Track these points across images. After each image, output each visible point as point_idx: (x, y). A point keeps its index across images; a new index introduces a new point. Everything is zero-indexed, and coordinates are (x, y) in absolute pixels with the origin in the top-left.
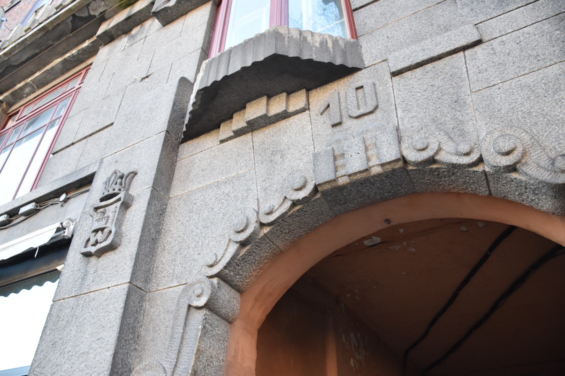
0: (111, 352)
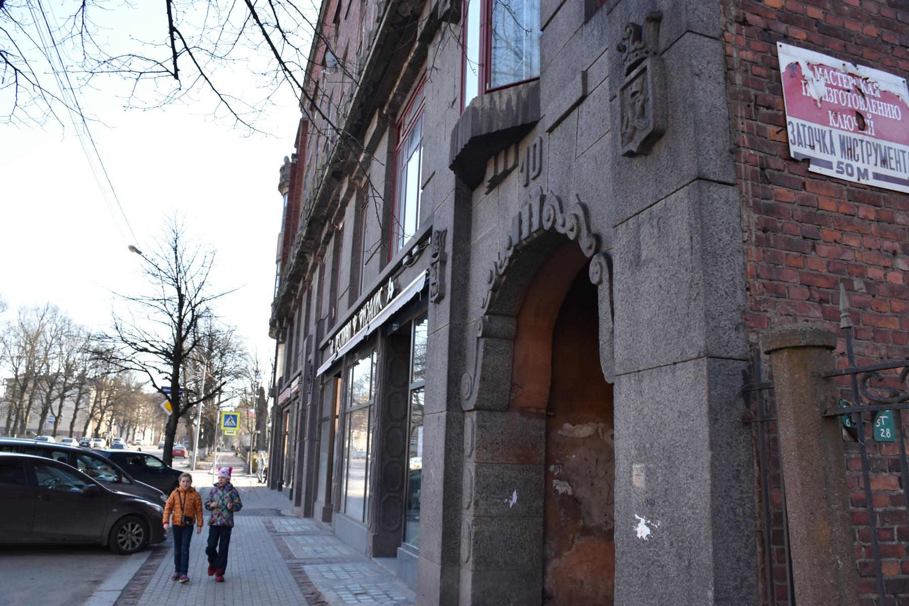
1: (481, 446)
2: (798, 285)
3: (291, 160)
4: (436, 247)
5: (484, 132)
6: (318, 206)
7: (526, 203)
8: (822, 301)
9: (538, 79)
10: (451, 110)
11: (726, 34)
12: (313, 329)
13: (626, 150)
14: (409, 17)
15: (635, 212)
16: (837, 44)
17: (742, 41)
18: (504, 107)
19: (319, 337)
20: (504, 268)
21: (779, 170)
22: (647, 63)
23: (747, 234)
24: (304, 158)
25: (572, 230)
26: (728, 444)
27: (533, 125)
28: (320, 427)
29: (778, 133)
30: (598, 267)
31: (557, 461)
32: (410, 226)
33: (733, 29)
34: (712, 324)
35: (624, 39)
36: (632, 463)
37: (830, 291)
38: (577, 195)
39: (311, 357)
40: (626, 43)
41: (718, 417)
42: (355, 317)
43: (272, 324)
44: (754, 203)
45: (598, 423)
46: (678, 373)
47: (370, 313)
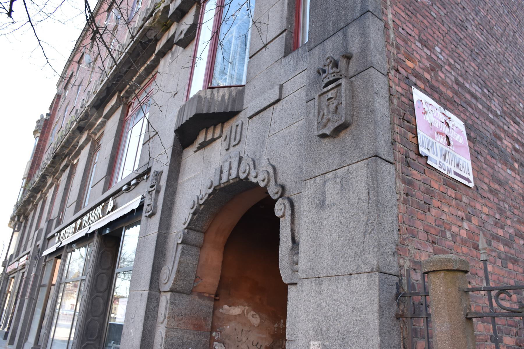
0: (152, 263)
1: (172, 316)
2: (422, 231)
3: (45, 117)
4: (154, 181)
5: (204, 112)
6: (62, 147)
7: (227, 161)
8: (433, 242)
9: (244, 86)
10: (173, 99)
11: (389, 74)
12: (43, 225)
13: (321, 132)
14: (152, 39)
15: (322, 173)
16: (436, 96)
17: (397, 81)
18: (220, 99)
19: (48, 230)
20: (204, 200)
21: (413, 160)
22: (343, 81)
23: (399, 195)
24: (54, 117)
25: (263, 180)
26: (389, 332)
27: (237, 113)
28: (38, 291)
29: (413, 138)
30: (283, 206)
31: (218, 330)
32: (129, 166)
33: (393, 72)
34: (382, 250)
35: (325, 66)
36: (310, 340)
37: (437, 237)
38: (268, 159)
39: (40, 243)
40: (326, 68)
41: (384, 313)
42: (79, 221)
43: (12, 219)
44: (402, 177)
45: (245, 306)
46: (353, 281)
47: (92, 219)
